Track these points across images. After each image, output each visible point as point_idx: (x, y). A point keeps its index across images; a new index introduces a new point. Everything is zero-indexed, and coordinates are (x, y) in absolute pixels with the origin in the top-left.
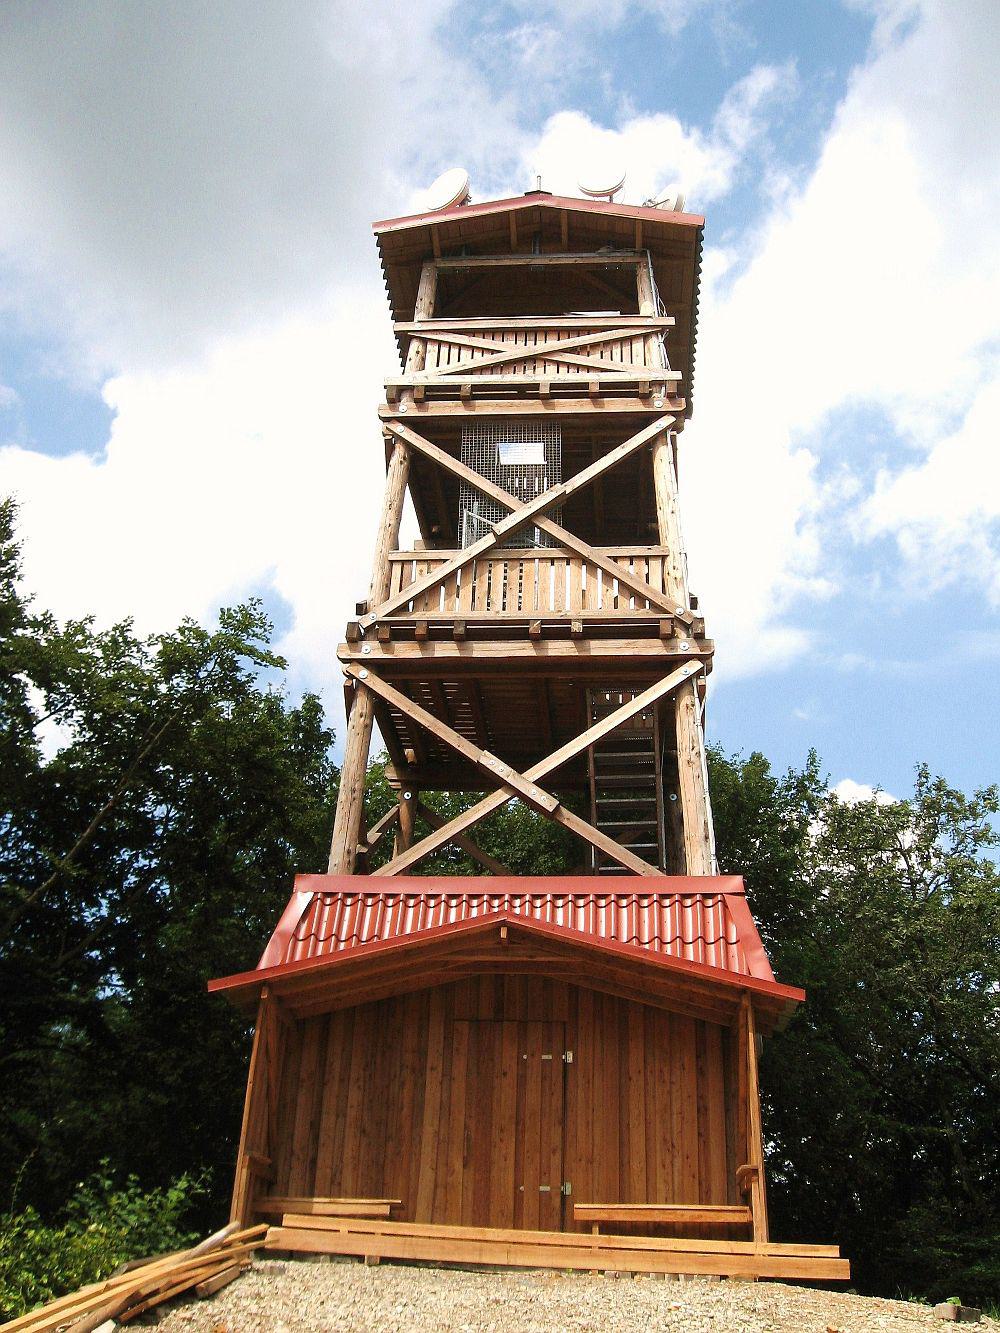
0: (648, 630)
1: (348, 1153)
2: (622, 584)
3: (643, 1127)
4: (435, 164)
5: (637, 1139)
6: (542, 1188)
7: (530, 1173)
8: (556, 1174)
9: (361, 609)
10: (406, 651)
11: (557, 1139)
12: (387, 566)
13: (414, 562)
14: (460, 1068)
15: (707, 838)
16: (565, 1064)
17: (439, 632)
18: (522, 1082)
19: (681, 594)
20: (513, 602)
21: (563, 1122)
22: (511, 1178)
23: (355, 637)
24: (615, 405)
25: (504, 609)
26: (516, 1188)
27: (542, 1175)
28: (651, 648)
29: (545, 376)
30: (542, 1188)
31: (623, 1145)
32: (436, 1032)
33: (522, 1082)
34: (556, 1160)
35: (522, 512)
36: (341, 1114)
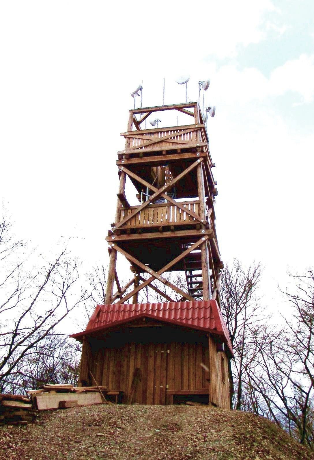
0: (192, 227)
1: (110, 379)
2: (141, 139)
3: (187, 369)
4: (269, 428)
5: (186, 373)
6: (161, 387)
7: (158, 383)
8: (164, 383)
9: (113, 225)
10: (124, 237)
11: (165, 374)
12: (119, 211)
13: (190, 205)
14: (139, 355)
15: (208, 288)
16: (167, 353)
17: (134, 231)
18: (155, 358)
19: (204, 215)
20: (155, 220)
21: (166, 369)
22: (152, 385)
23: (110, 234)
24: (187, 156)
25: (157, 221)
26: (154, 387)
27: (161, 383)
28: (193, 233)
29: (166, 147)
30: (161, 387)
31: (182, 366)
32: (133, 350)
33: (155, 358)
34: (165, 379)
35: (157, 193)
36: (108, 369)
